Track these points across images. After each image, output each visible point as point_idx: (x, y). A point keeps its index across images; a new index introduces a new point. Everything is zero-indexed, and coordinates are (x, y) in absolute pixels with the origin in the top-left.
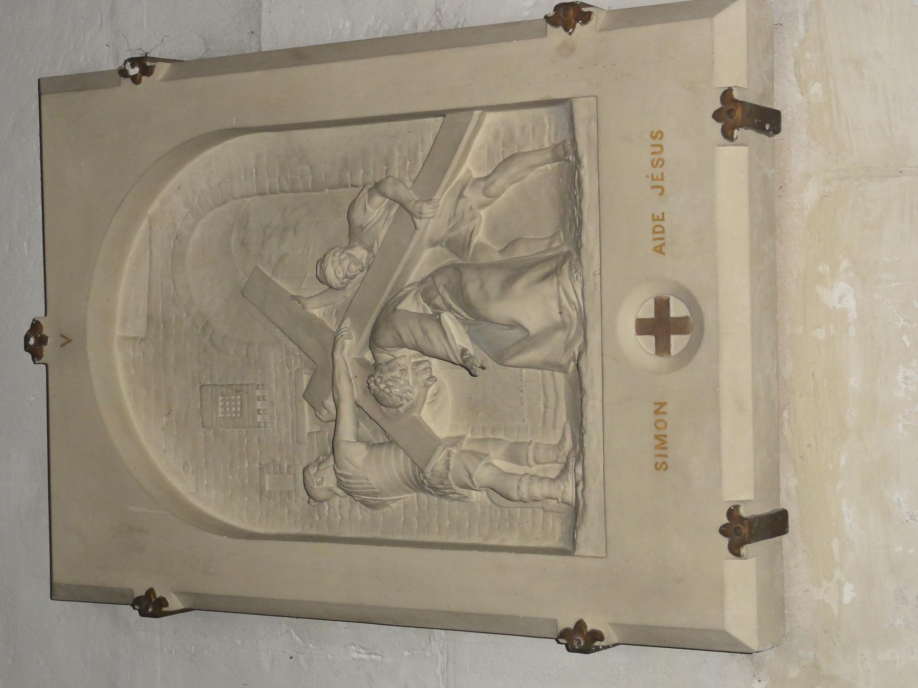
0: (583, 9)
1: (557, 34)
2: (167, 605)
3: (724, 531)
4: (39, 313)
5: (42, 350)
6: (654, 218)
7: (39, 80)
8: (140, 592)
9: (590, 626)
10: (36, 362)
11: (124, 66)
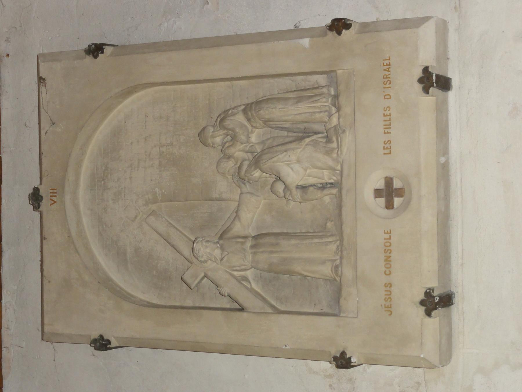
0: (347, 22)
1: (332, 35)
2: (110, 344)
4: (37, 184)
6: (386, 285)
7: (38, 54)
8: (95, 335)
10: (35, 210)
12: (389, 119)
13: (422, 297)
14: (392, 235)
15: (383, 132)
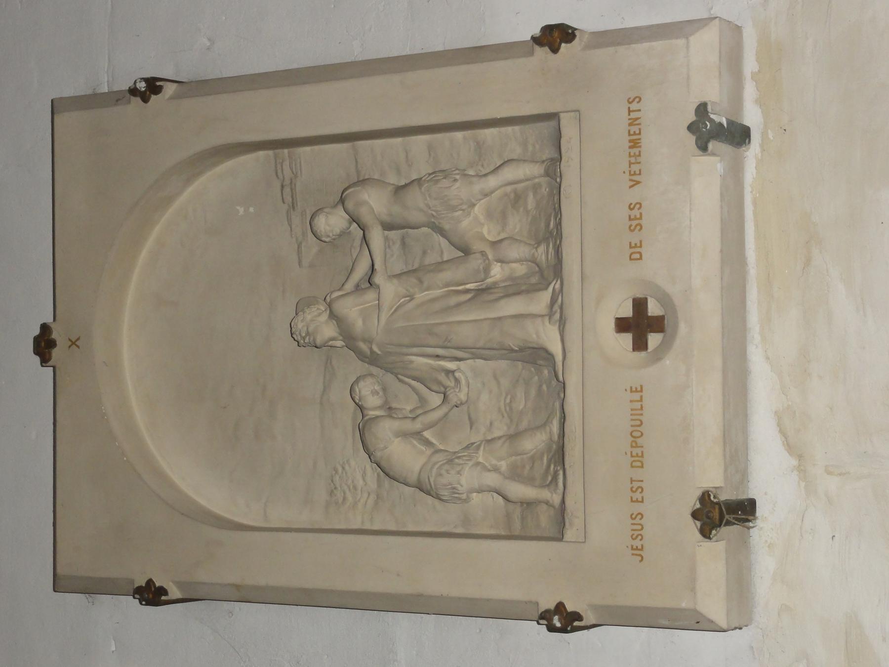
1: (542, 52)
3: (695, 515)
4: (49, 319)
5: (50, 354)
6: (632, 481)
7: (52, 100)
9: (570, 608)
11: (134, 86)
12: (639, 399)
13: (691, 117)
14: (644, 394)
15: (628, 218)
